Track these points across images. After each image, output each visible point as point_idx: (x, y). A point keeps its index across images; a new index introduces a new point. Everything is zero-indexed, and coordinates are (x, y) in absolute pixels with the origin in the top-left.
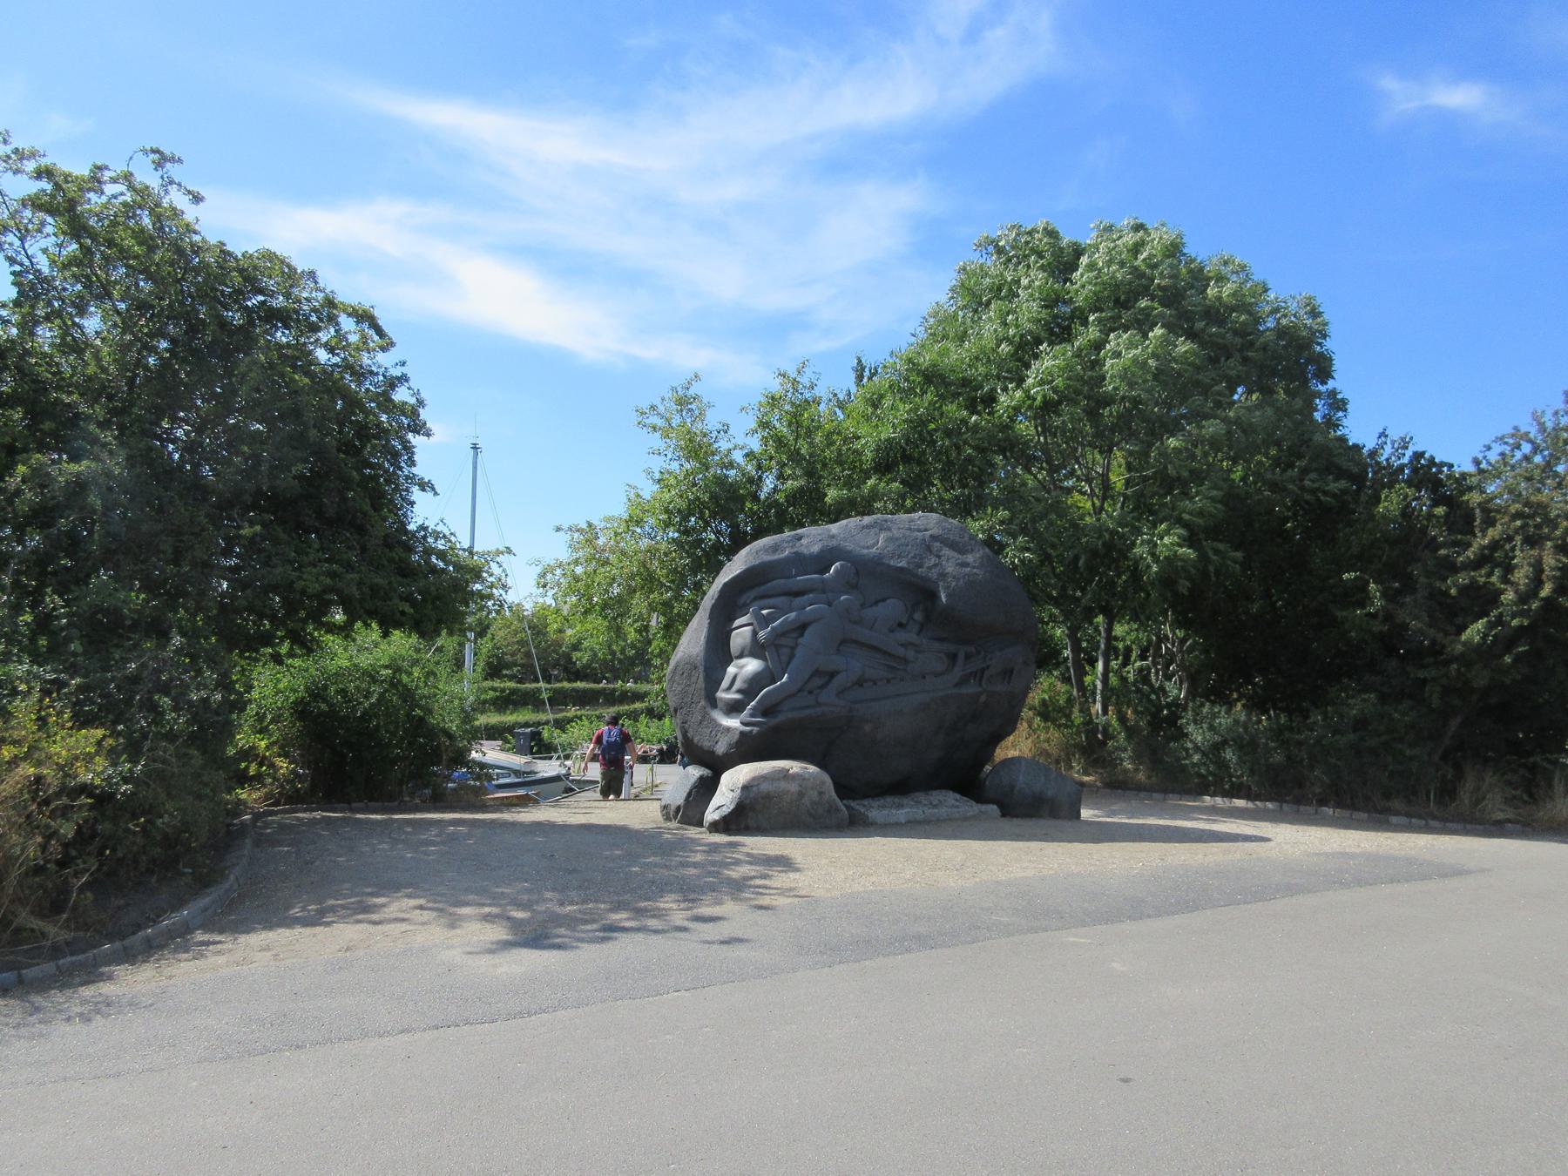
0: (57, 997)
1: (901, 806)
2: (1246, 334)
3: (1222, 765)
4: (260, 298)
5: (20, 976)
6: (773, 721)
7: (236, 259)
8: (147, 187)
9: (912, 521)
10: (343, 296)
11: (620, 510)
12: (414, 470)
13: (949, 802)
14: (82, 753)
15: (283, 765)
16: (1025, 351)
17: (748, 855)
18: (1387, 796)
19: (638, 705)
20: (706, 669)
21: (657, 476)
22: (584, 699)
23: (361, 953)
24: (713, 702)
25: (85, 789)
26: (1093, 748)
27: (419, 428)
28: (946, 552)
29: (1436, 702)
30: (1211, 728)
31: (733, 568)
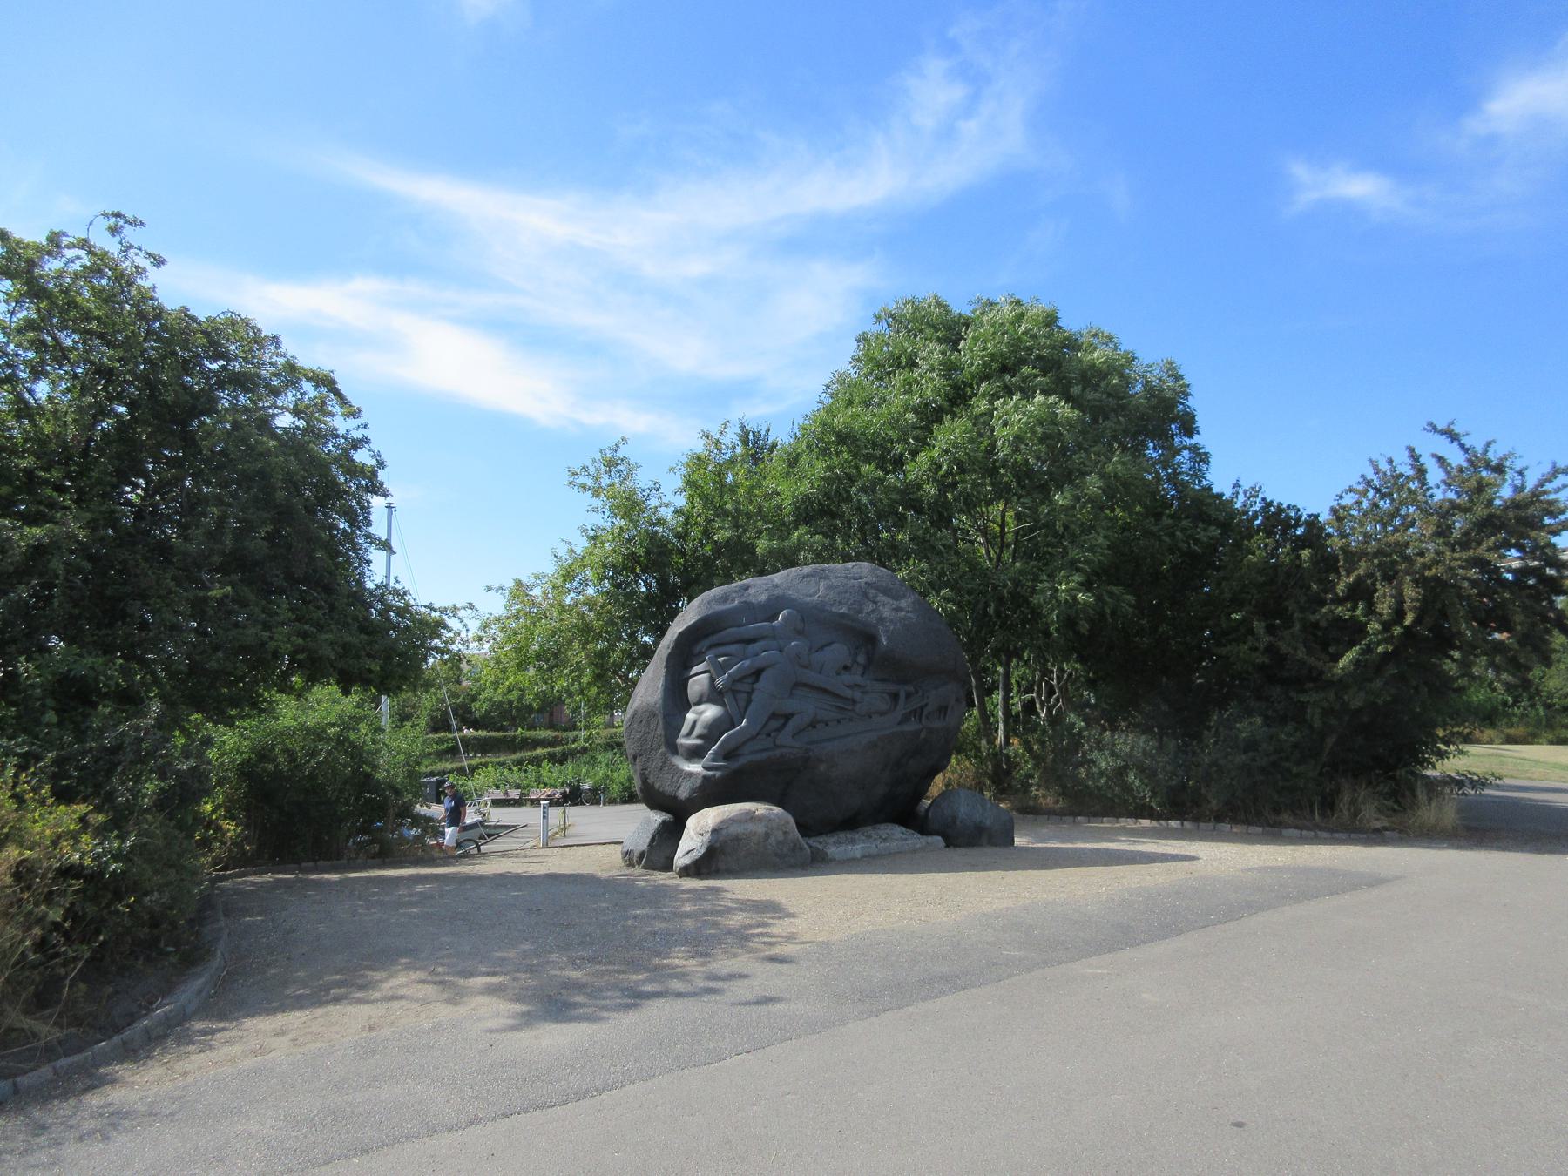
0: (64, 1108)
1: (853, 842)
2: (1120, 394)
3: (1127, 788)
4: (221, 363)
5: (15, 1084)
6: (735, 765)
7: (199, 323)
8: (106, 253)
9: (847, 569)
10: (305, 361)
11: (549, 568)
12: (370, 530)
13: (896, 834)
14: (60, 831)
15: (231, 828)
16: (931, 416)
17: (733, 901)
18: (1277, 811)
19: (539, 751)
20: (665, 717)
21: (592, 533)
22: (484, 747)
23: (386, 1032)
24: (674, 749)
25: (68, 872)
26: (1001, 777)
27: (376, 489)
28: (881, 598)
29: (1317, 724)
30: (1113, 754)
31: (689, 614)
